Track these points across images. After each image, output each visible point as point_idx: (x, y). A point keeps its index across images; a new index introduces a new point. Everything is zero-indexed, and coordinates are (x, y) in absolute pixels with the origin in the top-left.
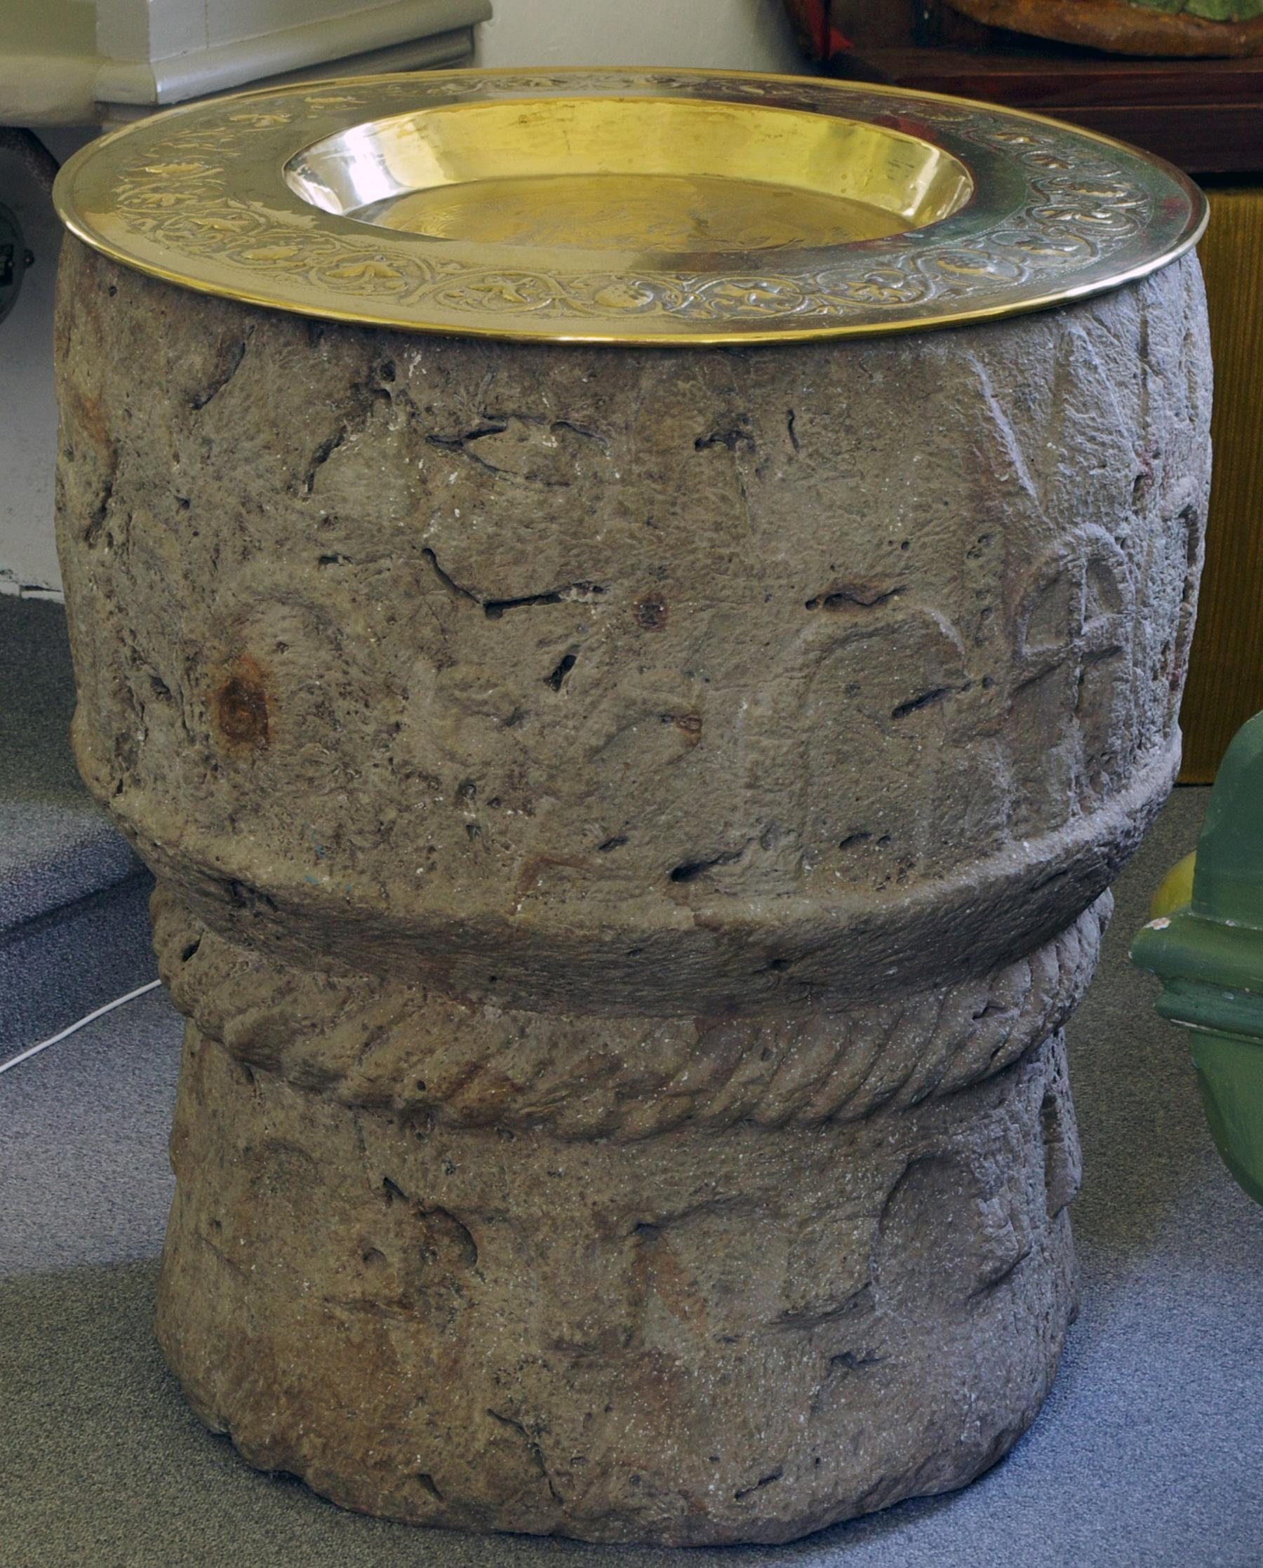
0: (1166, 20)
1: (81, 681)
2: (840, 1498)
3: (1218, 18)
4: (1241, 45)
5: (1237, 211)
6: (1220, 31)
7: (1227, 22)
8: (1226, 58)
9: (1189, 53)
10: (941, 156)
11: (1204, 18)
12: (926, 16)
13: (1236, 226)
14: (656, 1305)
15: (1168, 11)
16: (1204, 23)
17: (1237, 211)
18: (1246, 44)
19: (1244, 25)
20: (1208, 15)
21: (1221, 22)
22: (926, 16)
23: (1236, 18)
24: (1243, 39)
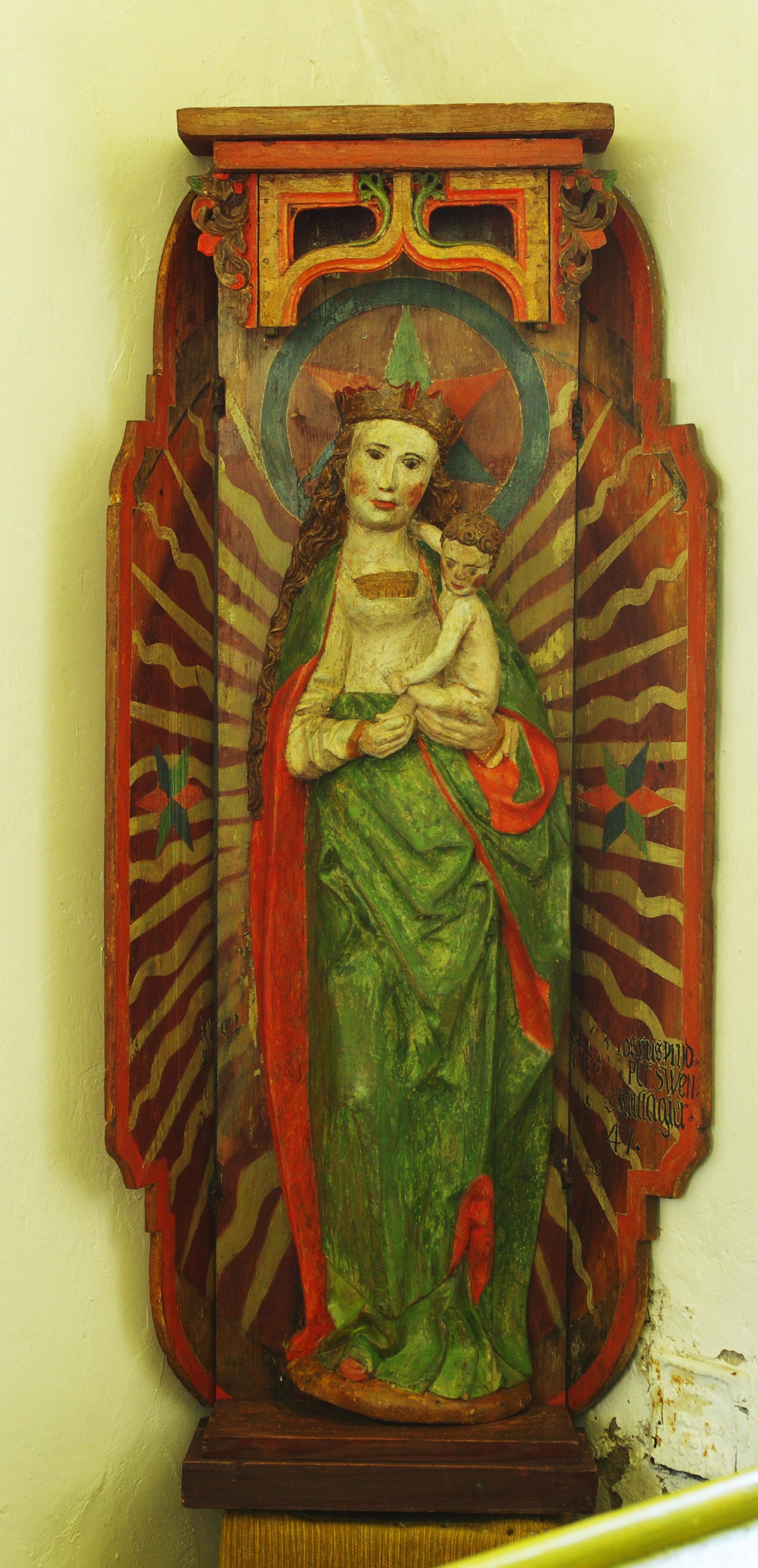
0: (414, 1397)
1: (655, 1353)
2: (533, 281)
3: (452, 1397)
4: (470, 1416)
5: (445, 1539)
6: (456, 1406)
7: (459, 1400)
8: (459, 1425)
9: (429, 1422)
10: (526, 315)
11: (443, 1397)
12: (281, 1380)
13: (444, 1549)
14: (563, 735)
15: (416, 1391)
16: (442, 1400)
17: (445, 1539)
18: (474, 1415)
19: (473, 1401)
20: (446, 1395)
21: (455, 1400)
22: (281, 1380)
23: (466, 1397)
24: (472, 1412)
